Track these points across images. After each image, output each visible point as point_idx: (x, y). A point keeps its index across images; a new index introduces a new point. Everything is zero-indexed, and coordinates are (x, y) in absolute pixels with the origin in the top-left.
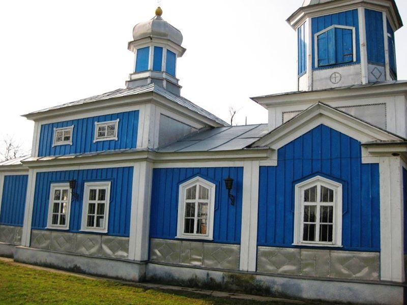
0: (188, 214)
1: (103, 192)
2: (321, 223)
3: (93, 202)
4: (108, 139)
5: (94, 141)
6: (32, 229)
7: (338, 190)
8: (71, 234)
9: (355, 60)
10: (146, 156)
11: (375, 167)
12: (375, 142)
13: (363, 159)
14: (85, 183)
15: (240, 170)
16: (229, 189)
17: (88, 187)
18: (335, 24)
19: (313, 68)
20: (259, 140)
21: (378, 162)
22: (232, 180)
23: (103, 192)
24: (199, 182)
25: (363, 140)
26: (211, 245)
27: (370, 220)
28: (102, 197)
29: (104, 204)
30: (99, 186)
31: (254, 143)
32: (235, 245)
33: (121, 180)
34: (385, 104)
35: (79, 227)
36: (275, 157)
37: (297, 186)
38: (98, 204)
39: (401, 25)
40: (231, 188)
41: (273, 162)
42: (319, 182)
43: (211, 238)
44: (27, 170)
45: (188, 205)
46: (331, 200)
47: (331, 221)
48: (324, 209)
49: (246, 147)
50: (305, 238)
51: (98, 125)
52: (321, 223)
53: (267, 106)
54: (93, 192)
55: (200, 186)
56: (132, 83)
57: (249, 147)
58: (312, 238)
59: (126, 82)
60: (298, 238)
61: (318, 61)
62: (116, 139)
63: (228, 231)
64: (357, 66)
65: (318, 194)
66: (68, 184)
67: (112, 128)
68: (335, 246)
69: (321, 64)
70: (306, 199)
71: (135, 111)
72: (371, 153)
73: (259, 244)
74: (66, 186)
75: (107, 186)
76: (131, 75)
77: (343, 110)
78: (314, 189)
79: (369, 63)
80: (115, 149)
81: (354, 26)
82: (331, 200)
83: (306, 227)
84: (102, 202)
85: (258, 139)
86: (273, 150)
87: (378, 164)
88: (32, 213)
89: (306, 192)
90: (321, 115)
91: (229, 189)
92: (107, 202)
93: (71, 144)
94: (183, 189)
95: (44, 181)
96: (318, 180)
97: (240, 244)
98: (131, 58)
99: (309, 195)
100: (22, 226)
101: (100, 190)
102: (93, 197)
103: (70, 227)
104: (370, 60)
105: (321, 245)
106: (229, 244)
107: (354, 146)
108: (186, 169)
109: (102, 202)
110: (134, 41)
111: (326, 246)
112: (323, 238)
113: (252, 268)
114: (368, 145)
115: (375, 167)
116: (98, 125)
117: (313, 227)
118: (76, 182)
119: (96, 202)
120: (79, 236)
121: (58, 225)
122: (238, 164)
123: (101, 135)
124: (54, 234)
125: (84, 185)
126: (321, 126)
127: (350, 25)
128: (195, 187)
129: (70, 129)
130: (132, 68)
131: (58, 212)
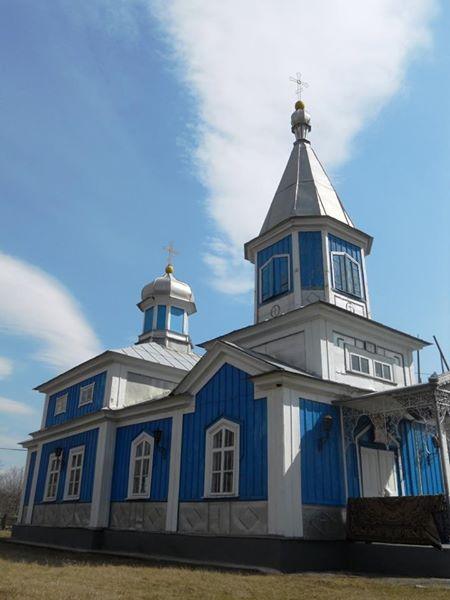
0: (217, 467)
5: (80, 405)
11: (264, 400)
23: (230, 435)
26: (238, 506)
28: (230, 442)
29: (232, 451)
33: (89, 440)
36: (193, 403)
38: (226, 452)
39: (369, 239)
41: (191, 409)
43: (237, 495)
54: (218, 437)
55: (227, 430)
63: (159, 494)
64: (291, 295)
67: (83, 399)
74: (151, 440)
79: (302, 289)
87: (266, 398)
92: (236, 448)
97: (267, 499)
102: (218, 444)
104: (304, 285)
113: (174, 529)
115: (264, 400)
119: (223, 449)
124: (214, 506)
128: (221, 432)
131: (225, 474)
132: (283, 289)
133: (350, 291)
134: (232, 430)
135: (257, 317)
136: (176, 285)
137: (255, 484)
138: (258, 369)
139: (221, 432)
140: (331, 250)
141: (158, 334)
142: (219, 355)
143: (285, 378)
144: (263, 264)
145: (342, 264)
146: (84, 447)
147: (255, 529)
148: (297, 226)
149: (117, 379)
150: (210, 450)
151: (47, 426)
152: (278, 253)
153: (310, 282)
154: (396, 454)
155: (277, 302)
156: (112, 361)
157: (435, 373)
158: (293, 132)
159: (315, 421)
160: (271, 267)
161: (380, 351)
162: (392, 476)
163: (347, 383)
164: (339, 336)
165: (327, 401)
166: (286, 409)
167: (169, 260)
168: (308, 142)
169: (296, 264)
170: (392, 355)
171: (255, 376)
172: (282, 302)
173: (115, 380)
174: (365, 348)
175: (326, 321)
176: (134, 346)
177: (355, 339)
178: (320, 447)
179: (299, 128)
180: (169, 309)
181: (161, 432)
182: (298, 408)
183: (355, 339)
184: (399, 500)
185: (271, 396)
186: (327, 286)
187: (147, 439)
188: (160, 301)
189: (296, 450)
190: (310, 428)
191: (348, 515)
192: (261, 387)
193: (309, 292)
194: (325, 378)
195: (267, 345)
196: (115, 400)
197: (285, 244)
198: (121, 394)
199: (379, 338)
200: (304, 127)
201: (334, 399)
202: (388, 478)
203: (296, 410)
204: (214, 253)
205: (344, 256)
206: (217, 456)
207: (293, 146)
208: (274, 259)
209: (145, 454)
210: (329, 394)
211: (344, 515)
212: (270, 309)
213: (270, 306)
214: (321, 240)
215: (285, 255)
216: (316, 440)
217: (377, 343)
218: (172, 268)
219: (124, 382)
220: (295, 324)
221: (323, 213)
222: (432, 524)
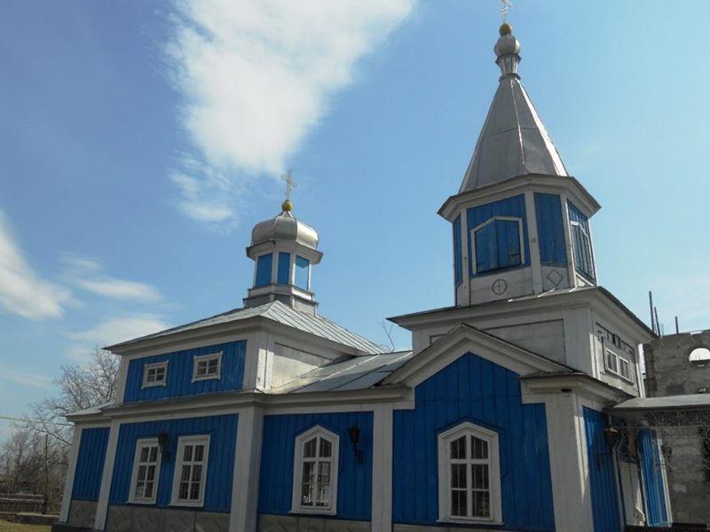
1: (200, 449)
2: (486, 490)
3: (187, 463)
4: (210, 378)
5: (193, 381)
6: (109, 504)
7: (492, 439)
8: (157, 510)
9: (523, 262)
10: (252, 400)
11: (540, 409)
12: (536, 375)
13: (523, 397)
14: (180, 438)
15: (369, 416)
16: (355, 443)
17: (183, 443)
18: (496, 215)
19: (471, 275)
20: (389, 376)
21: (543, 402)
22: (358, 431)
23: (200, 449)
24: (319, 433)
25: (522, 371)
26: (336, 524)
28: (199, 458)
29: (201, 466)
30: (197, 441)
31: (383, 380)
32: (365, 523)
33: (223, 430)
35: (168, 498)
36: (412, 397)
37: (441, 436)
38: (314, 456)
39: (597, 207)
40: (357, 441)
41: (409, 404)
42: (468, 430)
44: (109, 421)
45: (152, 478)
46: (486, 457)
47: (487, 486)
48: (476, 468)
49: (374, 385)
50: (455, 512)
51: (197, 359)
53: (409, 328)
54: (189, 449)
55: (322, 439)
56: (251, 301)
57: (377, 385)
58: (464, 513)
59: (244, 300)
60: (445, 511)
61: (477, 265)
62: (219, 377)
64: (527, 269)
65: (467, 444)
66: (157, 439)
68: (492, 523)
69: (480, 269)
70: (454, 456)
71: (241, 341)
72: (532, 389)
73: (394, 522)
75: (204, 441)
76: (249, 290)
77: (490, 332)
78: (463, 440)
79: (542, 264)
80: (195, 393)
81: (520, 217)
82: (486, 457)
83: (454, 494)
84: (199, 463)
85: (388, 374)
86: (409, 388)
87: (544, 404)
88: (500, 500)
89: (454, 444)
90: (466, 340)
91: (355, 443)
92: (204, 463)
93: (165, 384)
94: (300, 443)
95: (130, 434)
96: (467, 428)
97: (370, 521)
98: (250, 266)
99: (458, 449)
100: (97, 501)
101: (197, 447)
103: (157, 501)
105: (476, 523)
106: (356, 520)
107: (510, 381)
108: (313, 415)
109: (199, 463)
110: (255, 245)
111: (481, 523)
112: (477, 513)
114: (528, 378)
116: (197, 359)
117: (464, 494)
118: (167, 436)
119: (192, 463)
120: (169, 512)
121: (143, 497)
122: (366, 408)
123: (202, 372)
125: (177, 441)
126: (469, 354)
127: (516, 216)
128: (315, 440)
129: (164, 365)
130: (250, 283)
134: (483, 438)
136: (302, 229)
139: (315, 440)
141: (282, 290)
142: (462, 341)
144: (476, 225)
146: (209, 436)
149: (264, 351)
150: (137, 463)
151: (126, 400)
152: (501, 215)
153: (550, 256)
154: (639, 467)
156: (258, 329)
157: (71, 375)
164: (600, 329)
165: (596, 406)
166: (576, 418)
167: (287, 194)
168: (519, 78)
169: (533, 232)
170: (628, 349)
173: (262, 352)
176: (595, 324)
179: (508, 59)
180: (293, 258)
181: (356, 433)
186: (571, 264)
187: (152, 443)
188: (283, 246)
189: (587, 471)
192: (535, 391)
193: (551, 268)
194: (594, 376)
196: (262, 379)
198: (275, 374)
200: (514, 59)
204: (183, 170)
206: (186, 469)
207: (498, 84)
208: (496, 220)
209: (151, 461)
212: (491, 284)
214: (560, 207)
215: (516, 219)
217: (623, 338)
218: (291, 204)
219: (271, 354)
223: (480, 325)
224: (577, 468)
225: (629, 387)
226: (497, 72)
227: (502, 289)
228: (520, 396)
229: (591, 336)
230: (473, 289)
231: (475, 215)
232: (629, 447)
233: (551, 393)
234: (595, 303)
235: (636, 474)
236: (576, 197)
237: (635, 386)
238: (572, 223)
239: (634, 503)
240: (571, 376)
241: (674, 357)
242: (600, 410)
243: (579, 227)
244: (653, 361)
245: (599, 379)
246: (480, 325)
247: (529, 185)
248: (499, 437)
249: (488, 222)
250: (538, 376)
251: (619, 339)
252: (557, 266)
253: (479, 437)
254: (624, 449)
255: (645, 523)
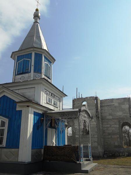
7: (6, 121)
9: (29, 71)
11: (20, 112)
25: (17, 100)
26: (5, 150)
27: (17, 134)
29: (4, 129)
34: (35, 87)
39: (55, 60)
43: (5, 146)
52: (91, 159)
61: (17, 72)
64: (30, 73)
77: (14, 91)
87: (22, 110)
88: (6, 139)
90: (4, 91)
97: (19, 148)
104: (35, 71)
107: (14, 103)
126: (4, 95)
132: (27, 71)
133: (48, 76)
134: (5, 121)
135: (14, 79)
137: (14, 142)
138: (20, 99)
140: (44, 61)
143: (31, 104)
144: (19, 61)
145: (47, 67)
147: (12, 159)
148: (35, 50)
152: (26, 58)
153: (37, 70)
154: (56, 130)
155: (23, 75)
158: (34, 18)
159: (37, 119)
160: (23, 62)
161: (55, 97)
162: (54, 137)
163: (48, 107)
164: (46, 91)
165: (41, 112)
166: (30, 115)
169: (33, 63)
170: (58, 98)
171: (18, 102)
172: (26, 75)
174: (52, 95)
175: (43, 85)
177: (50, 92)
178: (38, 129)
179: (36, 18)
182: (33, 115)
183: (50, 92)
184: (68, 145)
185: (24, 110)
189: (31, 130)
190: (36, 122)
191: (44, 151)
192: (20, 106)
194: (41, 104)
195: (19, 90)
197: (29, 56)
199: (56, 93)
201: (43, 112)
202: (29, 136)
203: (33, 115)
205: (48, 64)
208: (24, 60)
210: (42, 110)
211: (43, 150)
213: (20, 76)
214: (42, 57)
216: (37, 126)
217: (55, 94)
220: (32, 84)
221: (43, 48)
222: (74, 155)
223: (11, 89)
224: (27, 128)
225: (56, 108)
226: (33, 20)
227: (23, 79)
228: (16, 108)
229: (42, 92)
230: (16, 79)
231: (19, 58)
232: (83, 127)
233: (24, 107)
234: (43, 83)
235: (55, 132)
236: (47, 55)
237: (59, 108)
238: (45, 62)
239: (52, 139)
240: (30, 102)
241: (79, 104)
242: (42, 113)
243: (48, 64)
244: (74, 105)
245: (43, 105)
246: (11, 89)
247: (33, 50)
248: (9, 120)
249: (22, 60)
250: (22, 102)
251: (54, 95)
252: (38, 73)
253: (3, 121)
254: (128, 134)
255: (56, 145)
